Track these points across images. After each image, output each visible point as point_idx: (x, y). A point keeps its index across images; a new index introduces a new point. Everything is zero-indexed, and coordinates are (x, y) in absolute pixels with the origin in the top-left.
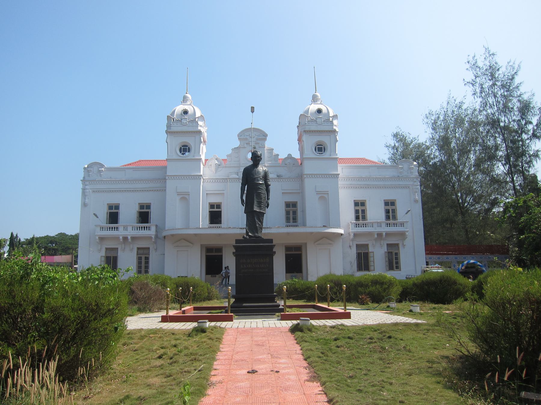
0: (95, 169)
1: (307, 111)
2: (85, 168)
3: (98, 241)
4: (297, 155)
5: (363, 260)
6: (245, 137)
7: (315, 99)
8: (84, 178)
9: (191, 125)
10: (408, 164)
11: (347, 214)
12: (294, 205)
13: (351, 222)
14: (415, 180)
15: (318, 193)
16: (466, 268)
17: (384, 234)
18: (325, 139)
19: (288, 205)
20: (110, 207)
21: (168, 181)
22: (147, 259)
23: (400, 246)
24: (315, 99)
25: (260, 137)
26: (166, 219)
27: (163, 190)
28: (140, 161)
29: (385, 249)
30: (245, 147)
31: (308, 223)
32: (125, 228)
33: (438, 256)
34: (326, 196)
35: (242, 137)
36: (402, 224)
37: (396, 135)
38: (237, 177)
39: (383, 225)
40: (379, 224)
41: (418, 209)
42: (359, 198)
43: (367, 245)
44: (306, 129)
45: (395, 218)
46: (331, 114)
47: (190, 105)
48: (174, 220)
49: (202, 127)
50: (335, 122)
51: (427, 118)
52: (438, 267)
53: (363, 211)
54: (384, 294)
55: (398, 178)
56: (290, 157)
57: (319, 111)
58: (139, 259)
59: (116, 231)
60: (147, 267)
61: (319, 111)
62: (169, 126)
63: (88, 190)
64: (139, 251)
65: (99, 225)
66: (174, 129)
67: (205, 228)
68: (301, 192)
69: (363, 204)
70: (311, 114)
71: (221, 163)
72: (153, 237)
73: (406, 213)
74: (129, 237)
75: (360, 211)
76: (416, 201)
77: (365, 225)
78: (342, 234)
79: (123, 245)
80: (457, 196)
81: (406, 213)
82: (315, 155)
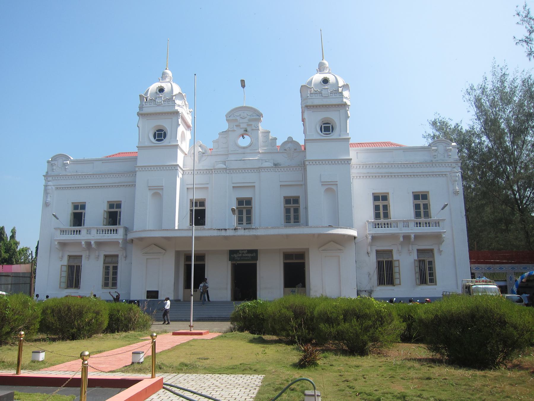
0: (60, 162)
1: (310, 82)
2: (48, 162)
3: (57, 247)
4: (300, 139)
5: (386, 273)
6: (234, 118)
7: (321, 68)
8: (47, 172)
9: (167, 104)
10: (445, 145)
11: (363, 211)
12: (296, 200)
13: (368, 221)
14: (454, 165)
15: (323, 184)
16: (528, 281)
17: (413, 236)
18: (333, 116)
19: (288, 200)
21: (138, 174)
22: (115, 268)
23: (436, 252)
24: (321, 68)
25: (254, 117)
26: (135, 220)
27: (133, 185)
29: (415, 256)
30: (234, 131)
31: (310, 224)
32: (89, 231)
33: (488, 265)
34: (334, 187)
35: (231, 118)
36: (437, 223)
37: (434, 124)
38: (224, 167)
39: (412, 225)
40: (406, 223)
41: (458, 205)
42: (380, 190)
43: (391, 251)
44: (308, 104)
45: (428, 216)
46: (341, 83)
47: (169, 82)
48: (143, 220)
49: (183, 108)
50: (346, 93)
51: (469, 94)
52: (486, 282)
53: (386, 207)
54: (366, 338)
55: (432, 163)
56: (290, 141)
57: (325, 81)
58: (107, 268)
59: (78, 235)
60: (115, 279)
61: (325, 81)
62: (141, 108)
63: (50, 187)
64: (107, 259)
65: (59, 228)
66: (146, 110)
67: (182, 230)
68: (304, 184)
69: (385, 198)
70: (315, 85)
71: (206, 151)
72: (120, 241)
73: (443, 209)
74: (93, 243)
75: (381, 205)
76: (456, 193)
77: (388, 225)
78: (355, 238)
79: (88, 252)
80: (513, 191)
81: (443, 209)
82: (322, 136)
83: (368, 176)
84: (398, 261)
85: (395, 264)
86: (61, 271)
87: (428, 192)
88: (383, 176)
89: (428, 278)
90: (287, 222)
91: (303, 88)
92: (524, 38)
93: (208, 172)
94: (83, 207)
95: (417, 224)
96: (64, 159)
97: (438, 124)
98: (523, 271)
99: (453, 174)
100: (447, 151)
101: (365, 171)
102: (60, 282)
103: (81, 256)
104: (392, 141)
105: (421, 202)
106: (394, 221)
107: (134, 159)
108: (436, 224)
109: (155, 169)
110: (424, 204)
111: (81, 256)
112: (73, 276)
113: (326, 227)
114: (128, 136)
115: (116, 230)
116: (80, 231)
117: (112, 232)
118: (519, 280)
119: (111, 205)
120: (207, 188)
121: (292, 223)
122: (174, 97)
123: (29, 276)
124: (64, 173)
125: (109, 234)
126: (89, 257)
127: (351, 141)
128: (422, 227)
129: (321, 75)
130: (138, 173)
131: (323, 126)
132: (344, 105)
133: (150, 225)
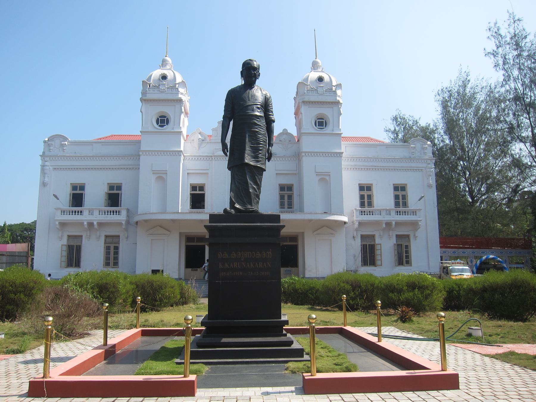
0: (57, 142)
2: (45, 142)
3: (58, 226)
4: (294, 132)
5: (369, 255)
7: (315, 66)
8: (44, 153)
11: (351, 200)
12: (290, 188)
13: (356, 209)
14: (429, 161)
15: (318, 174)
17: (394, 223)
19: (282, 188)
20: (74, 188)
22: (116, 248)
24: (315, 66)
27: (137, 168)
28: (368, 138)
31: (306, 210)
32: (91, 212)
33: (453, 250)
36: (414, 212)
37: (395, 119)
39: (393, 213)
40: (388, 212)
41: (432, 195)
42: (365, 181)
43: (373, 236)
44: (305, 100)
46: (334, 83)
47: (170, 69)
48: (148, 201)
49: (183, 94)
50: (339, 92)
53: (370, 197)
55: (410, 159)
57: (320, 79)
58: (108, 248)
59: (79, 216)
60: (116, 259)
61: (320, 79)
62: (144, 93)
63: (48, 168)
65: (60, 209)
66: (150, 96)
67: (184, 213)
68: (298, 173)
70: (311, 82)
71: (205, 138)
72: (124, 222)
73: (419, 200)
74: (95, 223)
75: (366, 195)
76: (430, 186)
77: (371, 213)
78: (345, 223)
79: (88, 232)
81: (419, 200)
83: (355, 168)
84: (380, 244)
85: (378, 247)
86: (62, 251)
87: (406, 185)
88: (368, 169)
89: (405, 260)
90: (281, 208)
91: (301, 85)
92: (492, 51)
93: (208, 159)
94: (82, 187)
95: (397, 212)
96: (61, 139)
97: (399, 120)
98: (482, 255)
99: (428, 170)
100: (423, 149)
101: (352, 163)
102: (61, 261)
103: (82, 236)
104: (372, 137)
105: (400, 193)
106: (378, 210)
107: (138, 143)
108: (70, 212)
109: (156, 154)
110: (368, 195)
111: (82, 236)
112: (73, 256)
113: (321, 214)
114: (130, 120)
115: (119, 212)
116: (81, 212)
117: (115, 213)
118: (478, 262)
119: (111, 187)
120: (207, 173)
121: (286, 209)
122: (177, 85)
123: (25, 255)
124: (61, 153)
125: (112, 215)
126: (89, 238)
127: (342, 136)
128: (401, 216)
129: (315, 73)
130: (141, 157)
131: (317, 121)
132: (338, 103)
133: (154, 209)
